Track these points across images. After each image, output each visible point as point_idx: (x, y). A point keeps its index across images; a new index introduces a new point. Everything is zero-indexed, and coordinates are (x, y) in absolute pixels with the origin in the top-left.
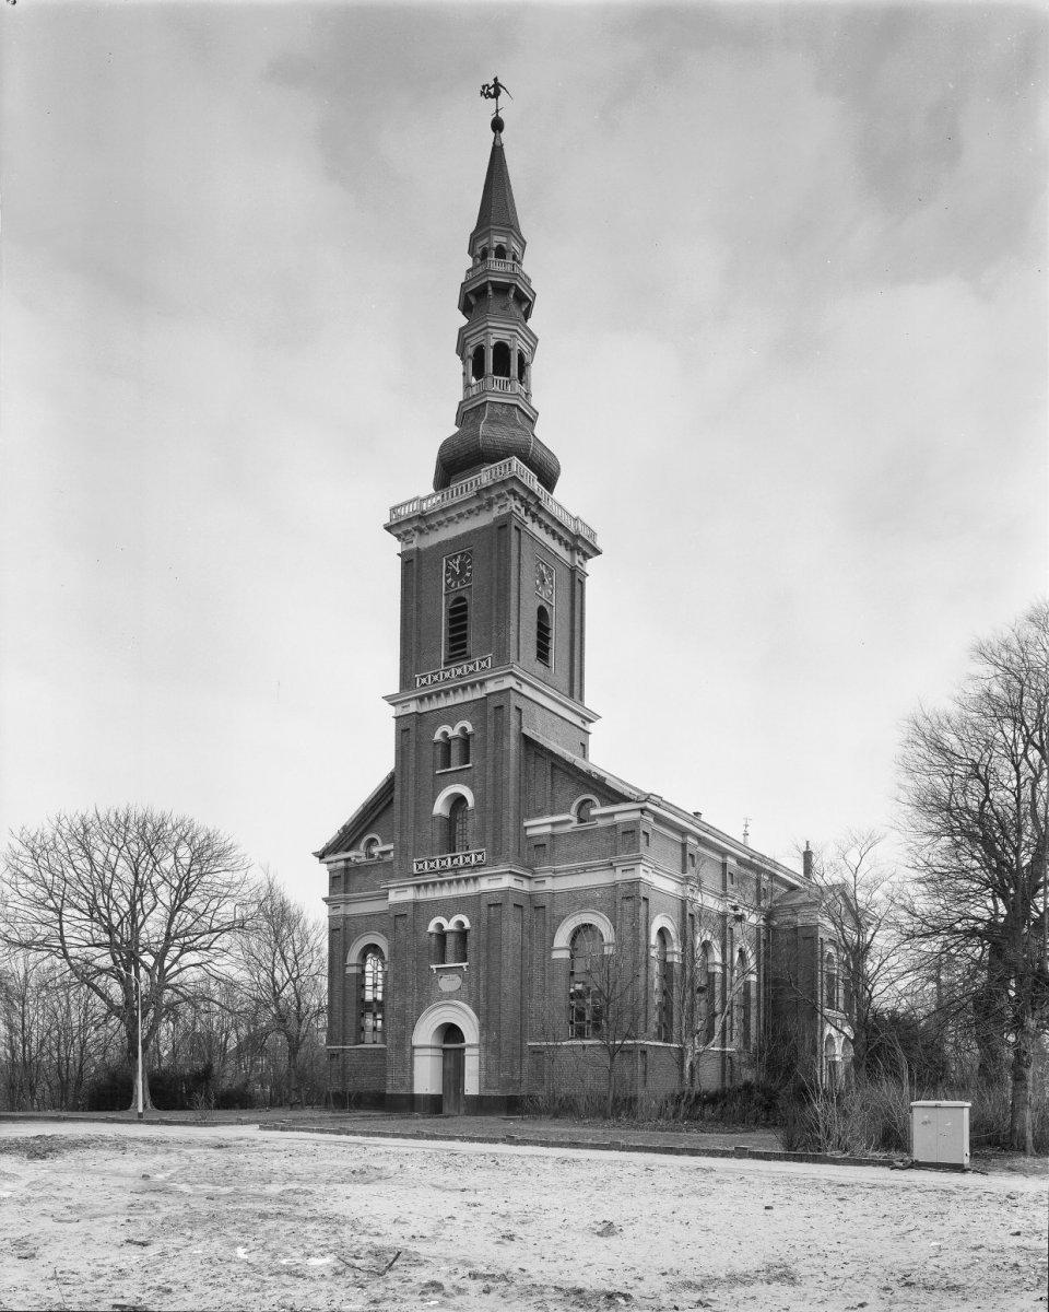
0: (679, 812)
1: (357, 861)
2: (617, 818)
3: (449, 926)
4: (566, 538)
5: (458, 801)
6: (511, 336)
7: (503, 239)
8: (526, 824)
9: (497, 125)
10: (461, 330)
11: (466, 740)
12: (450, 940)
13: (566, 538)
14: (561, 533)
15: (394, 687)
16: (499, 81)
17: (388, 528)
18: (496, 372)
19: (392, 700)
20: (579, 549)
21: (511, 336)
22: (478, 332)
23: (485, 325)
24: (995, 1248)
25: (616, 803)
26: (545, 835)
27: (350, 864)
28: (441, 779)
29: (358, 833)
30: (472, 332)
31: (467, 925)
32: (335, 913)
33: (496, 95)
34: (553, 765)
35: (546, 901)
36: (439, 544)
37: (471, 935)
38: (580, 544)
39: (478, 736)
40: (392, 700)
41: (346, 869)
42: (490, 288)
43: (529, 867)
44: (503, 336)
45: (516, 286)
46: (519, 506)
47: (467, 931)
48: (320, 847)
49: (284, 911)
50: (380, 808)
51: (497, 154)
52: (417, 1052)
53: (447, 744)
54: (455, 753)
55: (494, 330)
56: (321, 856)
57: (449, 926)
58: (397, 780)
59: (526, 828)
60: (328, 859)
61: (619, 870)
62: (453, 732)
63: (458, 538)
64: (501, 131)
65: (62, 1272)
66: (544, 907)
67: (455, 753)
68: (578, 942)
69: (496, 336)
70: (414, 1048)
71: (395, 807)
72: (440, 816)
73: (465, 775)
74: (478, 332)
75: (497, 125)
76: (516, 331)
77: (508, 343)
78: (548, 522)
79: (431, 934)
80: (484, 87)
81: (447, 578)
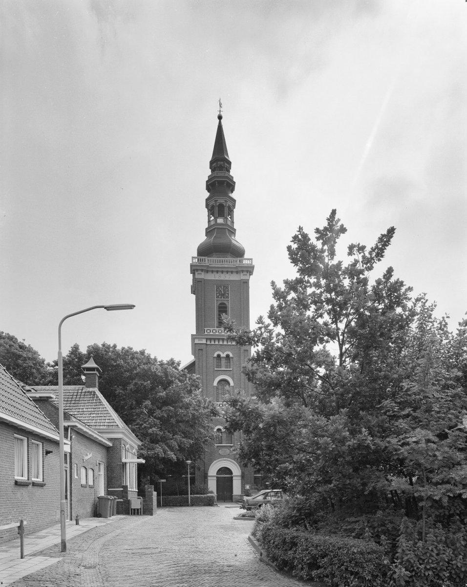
75: (220, 118)
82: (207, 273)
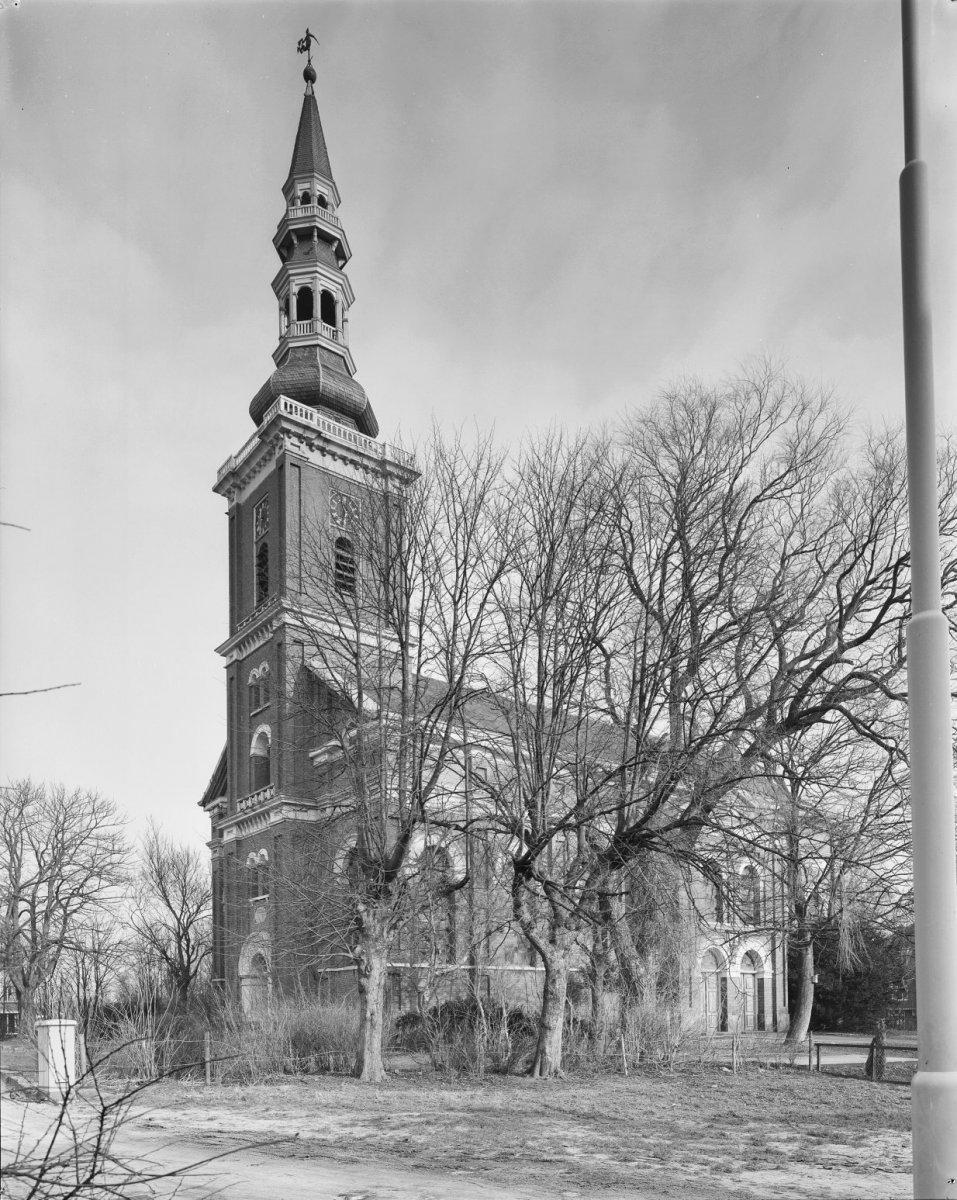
4: (371, 465)
7: (307, 185)
8: (311, 755)
9: (309, 76)
10: (274, 285)
13: (371, 465)
14: (366, 462)
15: (224, 634)
16: (310, 32)
17: (216, 490)
18: (300, 318)
19: (223, 650)
20: (390, 474)
22: (334, 281)
23: (314, 269)
24: (347, 1122)
30: (280, 285)
33: (307, 48)
36: (251, 497)
38: (388, 468)
40: (223, 650)
43: (312, 797)
44: (305, 280)
45: (317, 228)
46: (297, 443)
48: (200, 798)
49: (834, 941)
51: (309, 103)
55: (323, 278)
56: (203, 803)
59: (312, 758)
60: (209, 806)
63: (256, 492)
64: (313, 82)
69: (324, 283)
70: (241, 979)
74: (334, 281)
75: (309, 76)
76: (317, 272)
78: (340, 452)
80: (299, 43)
81: (257, 527)
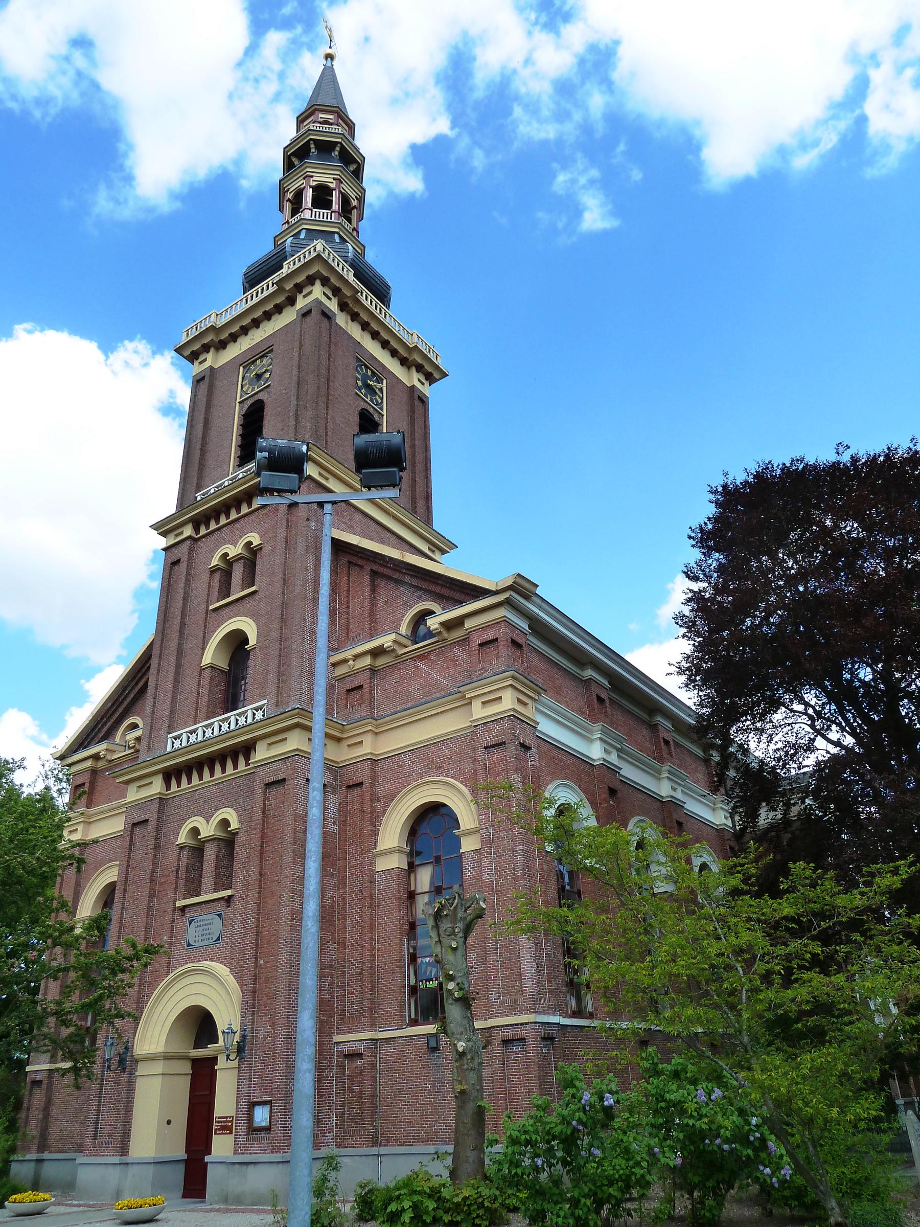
0: (544, 605)
1: (109, 757)
2: (469, 624)
3: (208, 829)
5: (237, 641)
6: (334, 179)
11: (252, 554)
12: (210, 853)
21: (334, 179)
25: (460, 603)
26: (362, 670)
27: (101, 764)
28: (212, 617)
29: (109, 724)
31: (234, 825)
32: (59, 833)
34: (374, 574)
35: (363, 775)
37: (240, 840)
39: (266, 549)
41: (94, 772)
42: (312, 146)
45: (311, 139)
47: (235, 834)
50: (129, 689)
52: (142, 1069)
53: (226, 570)
54: (238, 572)
57: (208, 829)
58: (156, 652)
61: (476, 705)
62: (233, 551)
65: (71, 864)
66: (361, 783)
67: (238, 572)
68: (424, 828)
71: (307, 1180)
72: (212, 667)
73: (249, 604)
77: (331, 185)
79: (181, 848)
82: (224, 348)
